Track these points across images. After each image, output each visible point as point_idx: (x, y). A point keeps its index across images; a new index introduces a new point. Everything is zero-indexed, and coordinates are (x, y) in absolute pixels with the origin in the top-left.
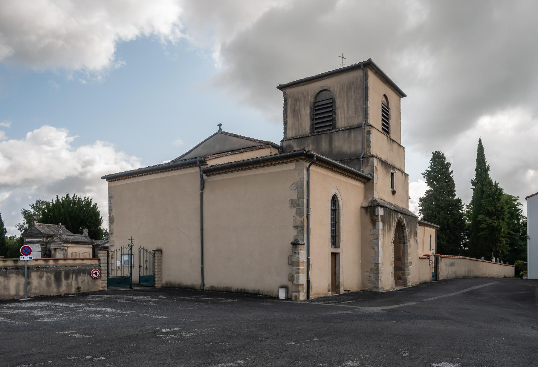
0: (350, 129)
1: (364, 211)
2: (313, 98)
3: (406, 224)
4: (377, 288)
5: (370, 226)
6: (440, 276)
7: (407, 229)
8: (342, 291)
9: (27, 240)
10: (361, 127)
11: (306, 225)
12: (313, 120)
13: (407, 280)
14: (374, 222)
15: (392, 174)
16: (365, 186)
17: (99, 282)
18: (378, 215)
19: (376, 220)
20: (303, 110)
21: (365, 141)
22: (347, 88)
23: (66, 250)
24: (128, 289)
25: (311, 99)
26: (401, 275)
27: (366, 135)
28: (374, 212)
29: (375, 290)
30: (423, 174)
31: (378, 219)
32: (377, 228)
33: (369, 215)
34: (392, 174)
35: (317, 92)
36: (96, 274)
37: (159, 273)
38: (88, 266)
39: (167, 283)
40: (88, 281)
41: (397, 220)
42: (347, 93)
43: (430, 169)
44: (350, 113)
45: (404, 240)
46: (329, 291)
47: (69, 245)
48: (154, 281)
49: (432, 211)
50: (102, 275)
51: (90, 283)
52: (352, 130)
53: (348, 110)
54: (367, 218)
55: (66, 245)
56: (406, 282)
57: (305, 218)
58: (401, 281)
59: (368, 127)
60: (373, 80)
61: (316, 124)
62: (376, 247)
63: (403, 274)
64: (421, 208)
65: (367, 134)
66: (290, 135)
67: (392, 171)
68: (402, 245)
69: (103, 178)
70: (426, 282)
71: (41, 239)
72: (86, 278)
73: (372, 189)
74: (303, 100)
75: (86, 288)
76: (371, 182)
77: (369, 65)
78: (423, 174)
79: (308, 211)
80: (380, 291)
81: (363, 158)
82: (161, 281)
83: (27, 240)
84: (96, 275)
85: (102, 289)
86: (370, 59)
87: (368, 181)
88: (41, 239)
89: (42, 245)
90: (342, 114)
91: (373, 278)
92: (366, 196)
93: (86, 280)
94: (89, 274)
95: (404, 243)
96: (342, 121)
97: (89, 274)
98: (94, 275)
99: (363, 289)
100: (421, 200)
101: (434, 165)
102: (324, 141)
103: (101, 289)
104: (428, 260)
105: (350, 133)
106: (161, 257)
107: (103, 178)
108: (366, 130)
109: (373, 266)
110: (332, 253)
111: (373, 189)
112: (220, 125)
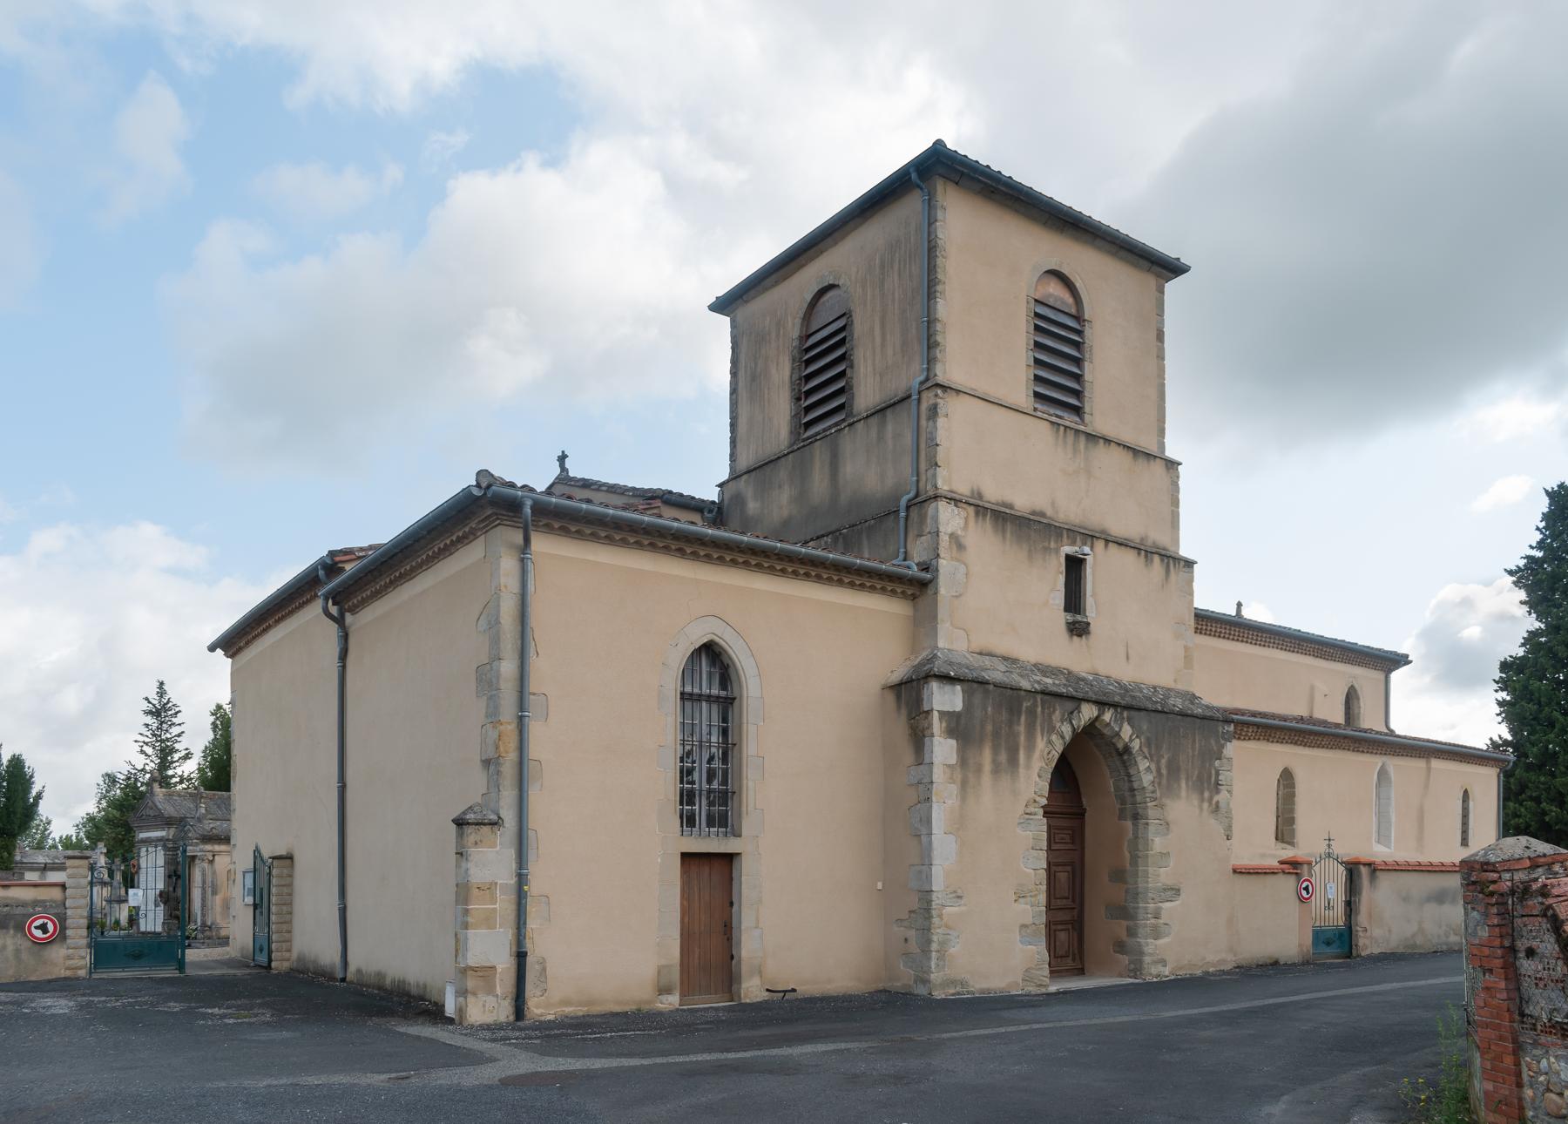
0: (881, 411)
1: (890, 697)
2: (798, 321)
3: (1136, 745)
4: (925, 982)
5: (908, 757)
6: (1361, 942)
7: (1143, 764)
8: (752, 990)
9: (143, 835)
10: (909, 397)
11: (511, 756)
12: (799, 399)
13: (1142, 953)
14: (919, 739)
15: (1075, 566)
16: (916, 609)
17: (58, 953)
18: (929, 712)
19: (923, 731)
20: (773, 371)
21: (923, 445)
22: (882, 266)
23: (211, 862)
24: (176, 974)
25: (794, 330)
26: (1123, 935)
27: (923, 422)
28: (919, 701)
29: (921, 990)
30: (1511, 573)
31: (930, 726)
32: (927, 760)
33: (904, 712)
34: (1075, 566)
35: (809, 297)
36: (43, 928)
37: (285, 927)
38: (24, 904)
39: (300, 959)
40: (17, 951)
41: (1067, 731)
42: (882, 282)
43: (1539, 554)
44: (890, 352)
45: (1134, 804)
46: (664, 990)
47: (217, 848)
48: (270, 952)
49: (1539, 703)
50: (69, 932)
51: (24, 956)
52: (889, 412)
53: (883, 345)
54: (900, 728)
55: (208, 847)
56: (1141, 962)
57: (510, 728)
58: (1125, 959)
59: (931, 394)
60: (960, 221)
61: (808, 409)
62: (924, 831)
63: (1132, 932)
64: (1503, 695)
65: (929, 419)
66: (744, 462)
67: (1068, 549)
68: (1129, 824)
69: (212, 648)
70: (1276, 963)
71: (163, 833)
72: (9, 942)
73: (933, 618)
74: (773, 335)
75: (11, 972)
76: (930, 592)
77: (938, 168)
78: (1511, 573)
79: (522, 704)
80: (938, 994)
81: (908, 508)
82: (289, 950)
83: (143, 835)
84: (45, 930)
85: (68, 973)
86: (939, 144)
87: (917, 587)
88: (163, 833)
89: (164, 846)
90: (870, 362)
91: (914, 947)
92: (914, 644)
93: (10, 948)
94: (20, 927)
95: (1136, 817)
96: (867, 391)
97: (20, 927)
98: (38, 933)
99: (888, 985)
100: (1504, 666)
101: (1554, 537)
102: (817, 465)
103: (64, 973)
104: (1292, 879)
105: (883, 424)
106: (291, 876)
107: (212, 648)
108: (924, 406)
109: (913, 902)
110: (683, 855)
111: (935, 617)
112: (562, 459)
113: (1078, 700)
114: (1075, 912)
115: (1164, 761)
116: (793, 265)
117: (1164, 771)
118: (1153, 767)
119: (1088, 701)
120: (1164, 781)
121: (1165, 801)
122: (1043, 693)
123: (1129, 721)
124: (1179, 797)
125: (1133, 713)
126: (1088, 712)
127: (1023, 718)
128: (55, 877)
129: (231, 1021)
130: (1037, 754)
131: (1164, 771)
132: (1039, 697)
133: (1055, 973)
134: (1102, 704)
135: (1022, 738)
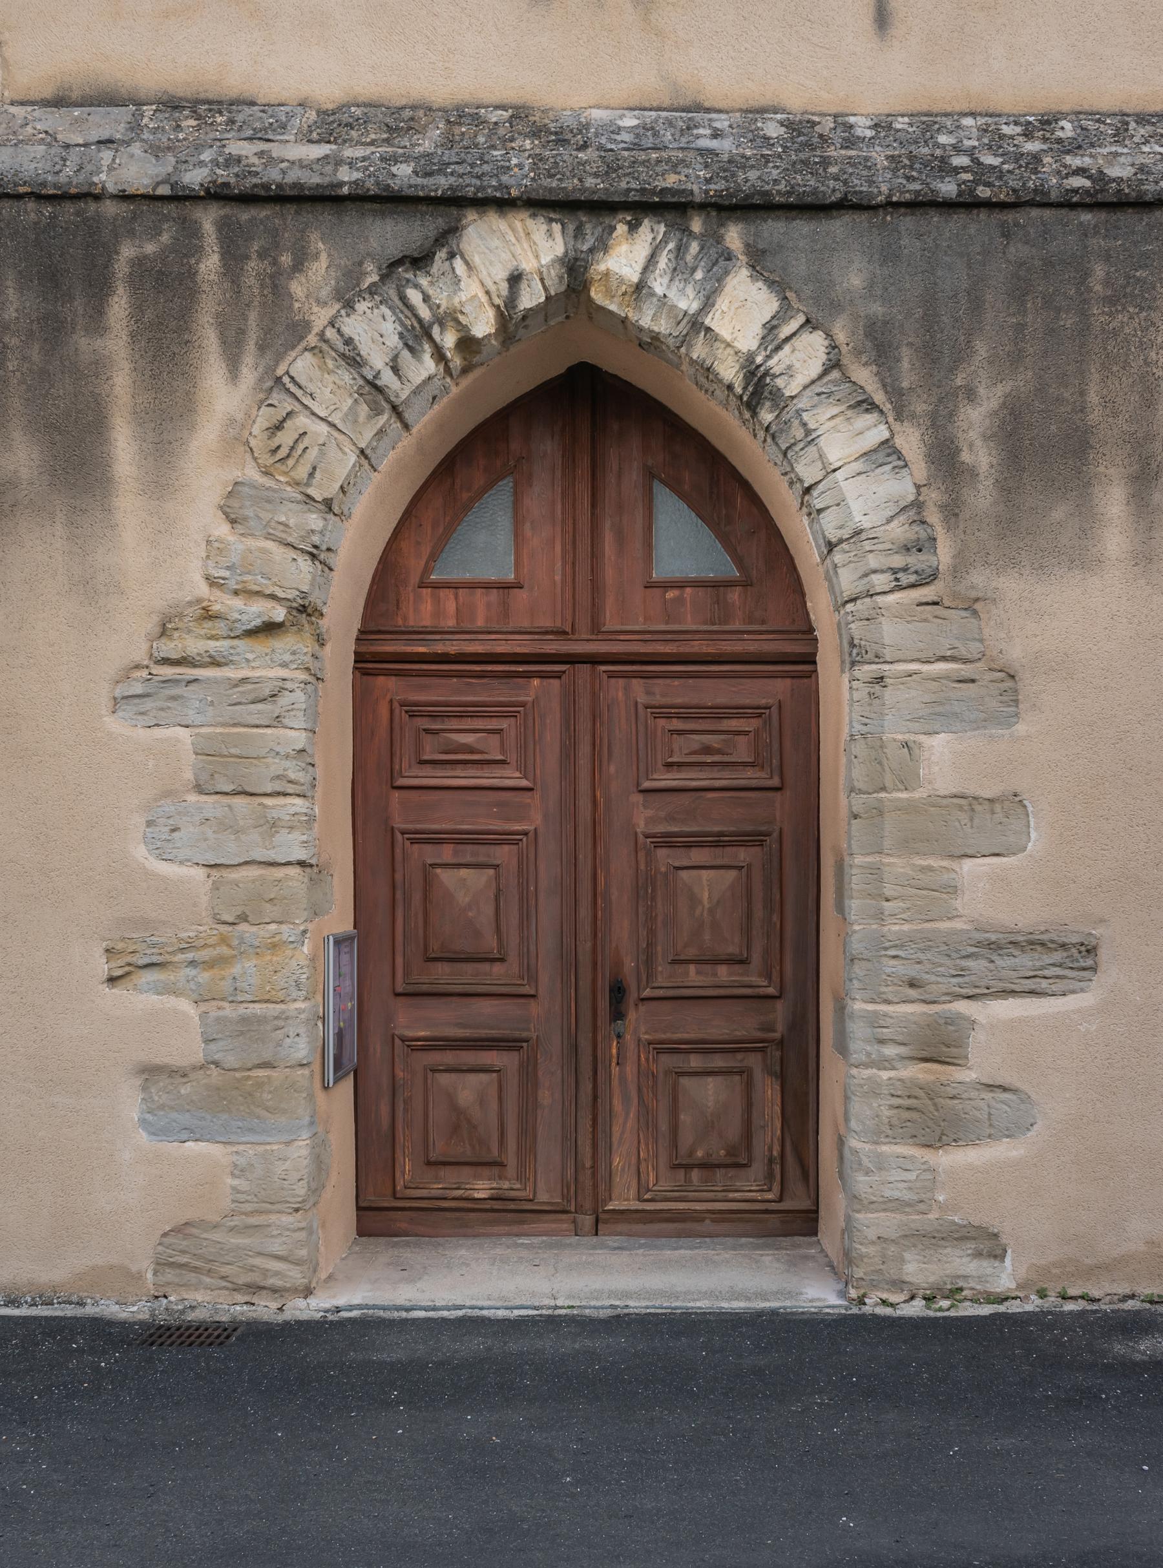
3: (802, 360)
113: (441, 211)
114: (780, 1013)
115: (974, 422)
116: (632, 658)
117: (980, 455)
118: (911, 441)
119: (504, 204)
120: (982, 497)
121: (978, 579)
122: (216, 194)
123: (759, 261)
124: (1082, 558)
125: (773, 228)
126: (503, 261)
127: (119, 306)
128: (443, 1020)
129: (614, 1051)
130: (207, 434)
131: (980, 455)
132: (208, 219)
133: (385, 1214)
134: (585, 210)
135: (122, 385)
